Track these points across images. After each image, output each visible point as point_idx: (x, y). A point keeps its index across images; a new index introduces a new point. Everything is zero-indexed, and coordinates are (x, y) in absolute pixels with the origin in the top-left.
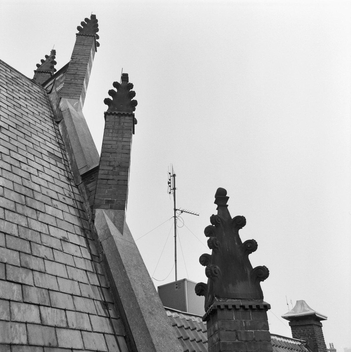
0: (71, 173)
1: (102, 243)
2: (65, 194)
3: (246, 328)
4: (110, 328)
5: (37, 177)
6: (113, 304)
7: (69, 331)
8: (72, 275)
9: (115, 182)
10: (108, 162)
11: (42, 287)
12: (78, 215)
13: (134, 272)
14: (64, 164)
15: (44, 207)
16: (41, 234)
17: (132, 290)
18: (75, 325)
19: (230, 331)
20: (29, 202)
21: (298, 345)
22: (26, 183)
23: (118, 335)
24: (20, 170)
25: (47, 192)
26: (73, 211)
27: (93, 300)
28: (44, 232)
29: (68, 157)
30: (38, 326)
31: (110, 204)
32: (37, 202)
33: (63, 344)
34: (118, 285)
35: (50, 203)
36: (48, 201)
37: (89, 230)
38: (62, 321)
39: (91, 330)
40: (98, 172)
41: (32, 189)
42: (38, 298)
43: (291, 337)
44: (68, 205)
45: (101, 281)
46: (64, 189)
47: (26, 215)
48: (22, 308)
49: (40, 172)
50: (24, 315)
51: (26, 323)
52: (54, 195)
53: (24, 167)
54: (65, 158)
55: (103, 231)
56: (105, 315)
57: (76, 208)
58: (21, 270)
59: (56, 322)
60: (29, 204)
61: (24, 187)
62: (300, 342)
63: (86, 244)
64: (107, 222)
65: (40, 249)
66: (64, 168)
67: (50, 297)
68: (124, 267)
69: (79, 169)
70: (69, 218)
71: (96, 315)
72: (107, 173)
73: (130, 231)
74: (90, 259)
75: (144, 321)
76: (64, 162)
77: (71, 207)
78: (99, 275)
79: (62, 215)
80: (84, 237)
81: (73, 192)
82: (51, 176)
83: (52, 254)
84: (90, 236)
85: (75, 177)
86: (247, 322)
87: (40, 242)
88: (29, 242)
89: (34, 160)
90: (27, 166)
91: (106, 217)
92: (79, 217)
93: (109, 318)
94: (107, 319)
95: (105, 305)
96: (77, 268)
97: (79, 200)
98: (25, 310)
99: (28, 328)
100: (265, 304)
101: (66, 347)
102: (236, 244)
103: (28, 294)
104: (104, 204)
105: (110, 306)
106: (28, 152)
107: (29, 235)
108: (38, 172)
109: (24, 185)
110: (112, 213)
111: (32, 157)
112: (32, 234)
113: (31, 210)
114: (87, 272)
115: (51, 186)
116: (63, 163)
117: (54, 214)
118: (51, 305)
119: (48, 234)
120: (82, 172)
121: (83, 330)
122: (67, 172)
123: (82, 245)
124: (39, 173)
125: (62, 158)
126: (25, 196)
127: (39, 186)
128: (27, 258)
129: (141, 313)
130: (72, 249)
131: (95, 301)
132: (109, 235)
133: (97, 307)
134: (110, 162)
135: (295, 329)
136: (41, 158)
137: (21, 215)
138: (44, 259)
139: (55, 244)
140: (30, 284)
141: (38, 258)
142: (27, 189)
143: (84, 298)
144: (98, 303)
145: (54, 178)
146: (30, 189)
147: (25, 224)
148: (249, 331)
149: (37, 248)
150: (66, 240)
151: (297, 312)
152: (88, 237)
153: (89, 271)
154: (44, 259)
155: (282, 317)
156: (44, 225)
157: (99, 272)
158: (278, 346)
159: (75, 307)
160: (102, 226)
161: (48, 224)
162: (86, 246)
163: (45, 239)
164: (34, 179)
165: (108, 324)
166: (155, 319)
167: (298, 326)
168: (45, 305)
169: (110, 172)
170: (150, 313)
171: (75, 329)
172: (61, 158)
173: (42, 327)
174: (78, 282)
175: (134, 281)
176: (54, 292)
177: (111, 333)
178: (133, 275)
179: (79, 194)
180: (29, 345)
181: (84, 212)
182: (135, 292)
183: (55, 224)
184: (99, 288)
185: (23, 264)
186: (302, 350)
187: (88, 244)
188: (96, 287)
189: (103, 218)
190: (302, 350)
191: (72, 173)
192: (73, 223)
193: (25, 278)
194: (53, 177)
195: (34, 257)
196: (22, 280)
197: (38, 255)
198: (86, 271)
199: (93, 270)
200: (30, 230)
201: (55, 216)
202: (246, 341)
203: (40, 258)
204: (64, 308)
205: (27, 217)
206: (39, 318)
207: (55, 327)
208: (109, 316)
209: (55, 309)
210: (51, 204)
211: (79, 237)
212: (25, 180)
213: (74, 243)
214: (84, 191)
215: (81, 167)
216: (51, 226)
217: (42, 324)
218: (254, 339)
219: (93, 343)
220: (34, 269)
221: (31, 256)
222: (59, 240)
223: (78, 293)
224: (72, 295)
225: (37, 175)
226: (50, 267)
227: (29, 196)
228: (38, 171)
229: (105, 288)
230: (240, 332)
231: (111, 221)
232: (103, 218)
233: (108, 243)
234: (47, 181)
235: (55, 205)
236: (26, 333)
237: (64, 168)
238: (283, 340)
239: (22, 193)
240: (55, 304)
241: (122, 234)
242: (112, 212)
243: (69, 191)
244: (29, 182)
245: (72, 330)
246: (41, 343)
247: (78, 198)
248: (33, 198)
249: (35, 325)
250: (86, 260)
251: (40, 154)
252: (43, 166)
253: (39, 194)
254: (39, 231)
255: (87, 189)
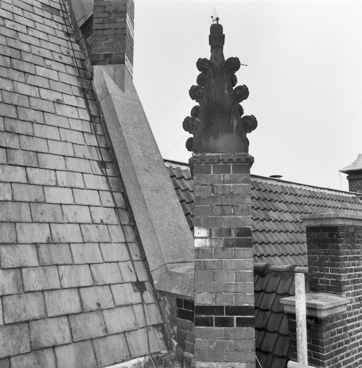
0: (71, 27)
1: (101, 102)
2: (62, 53)
3: (224, 182)
4: (106, 185)
5: (25, 35)
6: (112, 163)
7: (58, 189)
8: (66, 137)
9: (112, 32)
10: (103, 8)
11: (29, 150)
12: (78, 75)
13: (132, 131)
14: (63, 16)
15: (34, 69)
16: (30, 97)
17: (127, 149)
18: (66, 183)
19: (206, 185)
20: (15, 64)
21: (352, 197)
22: (12, 43)
23: (115, 192)
24: (4, 28)
25: (39, 52)
26: (70, 70)
27: (89, 160)
28: (34, 95)
29: (67, 7)
30: (24, 185)
31: (108, 59)
32: (25, 63)
33: (51, 200)
34: (114, 145)
35: (42, 63)
36: (40, 61)
37: (89, 90)
38: (51, 180)
39: (84, 188)
40: (92, 20)
41: (19, 49)
42: (24, 160)
43: (348, 190)
44: (65, 64)
45: (100, 142)
46: (61, 47)
47: (11, 79)
48: (6, 170)
49: (30, 29)
50: (9, 176)
51: (11, 183)
52: (48, 54)
53: (9, 24)
54: (64, 10)
55: (101, 89)
56: (101, 174)
57: (75, 67)
58: (5, 134)
59: (45, 182)
60: (15, 66)
61: (9, 48)
62: (356, 194)
63: (85, 105)
64: (106, 79)
65: (28, 113)
66: (63, 22)
67: (38, 159)
68: (120, 126)
69: (77, 20)
70: (65, 78)
71: (91, 174)
72: (102, 22)
73: (134, 88)
74: (89, 120)
75: (136, 177)
76: (63, 14)
77: (68, 66)
78: (98, 136)
79: (57, 76)
80: (84, 98)
81: (72, 49)
82: (45, 33)
83: (42, 118)
84: (91, 97)
85: (76, 31)
86: (226, 177)
87: (28, 106)
88: (15, 107)
89: (22, 15)
90: (13, 23)
91: (105, 73)
92: (79, 77)
93: (106, 176)
94: (104, 177)
95: (102, 164)
96: (72, 130)
97: (80, 58)
98: (10, 171)
99: (13, 187)
100: (249, 156)
101: (55, 203)
102: (226, 92)
103: (13, 157)
104: (102, 59)
105: (109, 166)
106: (15, 6)
107: (15, 99)
108: (27, 29)
109: (9, 45)
110: (112, 70)
111: (19, 12)
112: (18, 98)
113: (18, 73)
114: (85, 134)
115: (44, 44)
116: (62, 15)
117: (47, 76)
118: (39, 166)
119: (39, 97)
120: (80, 24)
121: (74, 188)
122: (66, 26)
123: (80, 106)
124: (28, 31)
125: (61, 9)
126: (10, 58)
127: (28, 45)
128: (13, 123)
129: (134, 171)
130: (68, 111)
131: (91, 161)
132: (107, 93)
133: (93, 166)
134: (105, 7)
135: (353, 183)
136: (32, 11)
137: (6, 78)
138: (32, 123)
139: (46, 106)
140: (15, 148)
141: (26, 122)
142: (13, 50)
143: (77, 159)
144: (95, 163)
145: (48, 35)
146: (16, 50)
147: (11, 89)
148: (227, 185)
149: (24, 113)
150: (60, 102)
151: (357, 166)
152: (88, 97)
153: (86, 132)
154: (32, 123)
155: (340, 171)
156: (33, 88)
157: (99, 133)
158: (323, 198)
159: (67, 168)
160: (100, 85)
161: (38, 87)
162: (84, 107)
163: (35, 103)
164: (23, 37)
165: (104, 182)
166: (151, 175)
167: (356, 179)
168: (32, 166)
169: (106, 20)
170: (145, 170)
171: (65, 187)
172: (59, 10)
173: (28, 185)
174: (72, 143)
175: (130, 140)
176: (44, 154)
177: (107, 189)
178: (130, 135)
179: (80, 50)
180: (13, 201)
181: (86, 71)
182: (130, 150)
183: (47, 86)
184: (97, 148)
185: (8, 129)
186: (355, 202)
187: (87, 104)
188: (94, 148)
189: (102, 75)
190: (355, 202)
191: (72, 26)
192: (70, 83)
193: (10, 142)
194: (47, 34)
195: (20, 121)
196: (6, 144)
197: (25, 119)
198: (83, 132)
199: (92, 131)
200: (17, 94)
201: (48, 77)
202: (223, 195)
203: (28, 123)
204: (54, 169)
205: (13, 81)
206: (26, 178)
207: (43, 186)
208: (105, 175)
209: (44, 170)
210: (43, 65)
211: (77, 98)
212: (11, 39)
213: (70, 104)
214: (85, 46)
215: (80, 18)
216: (42, 89)
217: (28, 183)
218: (232, 193)
219: (86, 199)
220: (20, 133)
221: (18, 121)
222: (52, 103)
223: (72, 154)
224: (64, 156)
225: (26, 33)
226: (39, 130)
227: (15, 58)
228: (28, 28)
229: (104, 148)
230: (217, 186)
231: (111, 77)
232: (102, 75)
233: (106, 102)
234: (39, 39)
235: (48, 66)
236: (11, 191)
237: (63, 22)
238: (334, 193)
239: (6, 55)
240: (43, 165)
241: (123, 91)
242: (111, 68)
243: (68, 48)
244: (16, 42)
245: (62, 188)
246: (27, 199)
247: (78, 55)
248: (21, 59)
249: (21, 184)
250: (84, 121)
251: (31, 7)
252: (34, 21)
253: (29, 54)
254: (28, 94)
255: (87, 44)
